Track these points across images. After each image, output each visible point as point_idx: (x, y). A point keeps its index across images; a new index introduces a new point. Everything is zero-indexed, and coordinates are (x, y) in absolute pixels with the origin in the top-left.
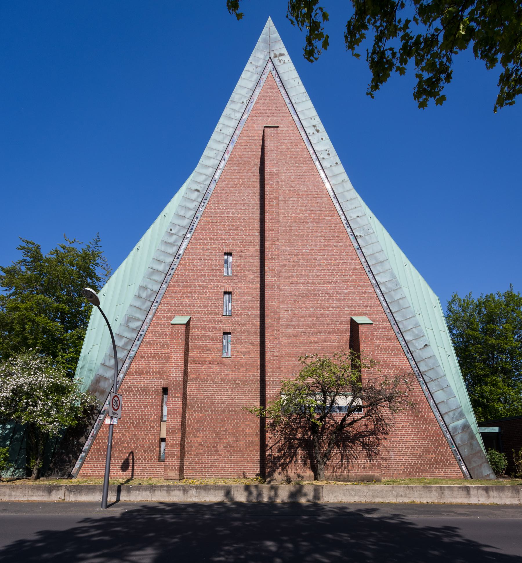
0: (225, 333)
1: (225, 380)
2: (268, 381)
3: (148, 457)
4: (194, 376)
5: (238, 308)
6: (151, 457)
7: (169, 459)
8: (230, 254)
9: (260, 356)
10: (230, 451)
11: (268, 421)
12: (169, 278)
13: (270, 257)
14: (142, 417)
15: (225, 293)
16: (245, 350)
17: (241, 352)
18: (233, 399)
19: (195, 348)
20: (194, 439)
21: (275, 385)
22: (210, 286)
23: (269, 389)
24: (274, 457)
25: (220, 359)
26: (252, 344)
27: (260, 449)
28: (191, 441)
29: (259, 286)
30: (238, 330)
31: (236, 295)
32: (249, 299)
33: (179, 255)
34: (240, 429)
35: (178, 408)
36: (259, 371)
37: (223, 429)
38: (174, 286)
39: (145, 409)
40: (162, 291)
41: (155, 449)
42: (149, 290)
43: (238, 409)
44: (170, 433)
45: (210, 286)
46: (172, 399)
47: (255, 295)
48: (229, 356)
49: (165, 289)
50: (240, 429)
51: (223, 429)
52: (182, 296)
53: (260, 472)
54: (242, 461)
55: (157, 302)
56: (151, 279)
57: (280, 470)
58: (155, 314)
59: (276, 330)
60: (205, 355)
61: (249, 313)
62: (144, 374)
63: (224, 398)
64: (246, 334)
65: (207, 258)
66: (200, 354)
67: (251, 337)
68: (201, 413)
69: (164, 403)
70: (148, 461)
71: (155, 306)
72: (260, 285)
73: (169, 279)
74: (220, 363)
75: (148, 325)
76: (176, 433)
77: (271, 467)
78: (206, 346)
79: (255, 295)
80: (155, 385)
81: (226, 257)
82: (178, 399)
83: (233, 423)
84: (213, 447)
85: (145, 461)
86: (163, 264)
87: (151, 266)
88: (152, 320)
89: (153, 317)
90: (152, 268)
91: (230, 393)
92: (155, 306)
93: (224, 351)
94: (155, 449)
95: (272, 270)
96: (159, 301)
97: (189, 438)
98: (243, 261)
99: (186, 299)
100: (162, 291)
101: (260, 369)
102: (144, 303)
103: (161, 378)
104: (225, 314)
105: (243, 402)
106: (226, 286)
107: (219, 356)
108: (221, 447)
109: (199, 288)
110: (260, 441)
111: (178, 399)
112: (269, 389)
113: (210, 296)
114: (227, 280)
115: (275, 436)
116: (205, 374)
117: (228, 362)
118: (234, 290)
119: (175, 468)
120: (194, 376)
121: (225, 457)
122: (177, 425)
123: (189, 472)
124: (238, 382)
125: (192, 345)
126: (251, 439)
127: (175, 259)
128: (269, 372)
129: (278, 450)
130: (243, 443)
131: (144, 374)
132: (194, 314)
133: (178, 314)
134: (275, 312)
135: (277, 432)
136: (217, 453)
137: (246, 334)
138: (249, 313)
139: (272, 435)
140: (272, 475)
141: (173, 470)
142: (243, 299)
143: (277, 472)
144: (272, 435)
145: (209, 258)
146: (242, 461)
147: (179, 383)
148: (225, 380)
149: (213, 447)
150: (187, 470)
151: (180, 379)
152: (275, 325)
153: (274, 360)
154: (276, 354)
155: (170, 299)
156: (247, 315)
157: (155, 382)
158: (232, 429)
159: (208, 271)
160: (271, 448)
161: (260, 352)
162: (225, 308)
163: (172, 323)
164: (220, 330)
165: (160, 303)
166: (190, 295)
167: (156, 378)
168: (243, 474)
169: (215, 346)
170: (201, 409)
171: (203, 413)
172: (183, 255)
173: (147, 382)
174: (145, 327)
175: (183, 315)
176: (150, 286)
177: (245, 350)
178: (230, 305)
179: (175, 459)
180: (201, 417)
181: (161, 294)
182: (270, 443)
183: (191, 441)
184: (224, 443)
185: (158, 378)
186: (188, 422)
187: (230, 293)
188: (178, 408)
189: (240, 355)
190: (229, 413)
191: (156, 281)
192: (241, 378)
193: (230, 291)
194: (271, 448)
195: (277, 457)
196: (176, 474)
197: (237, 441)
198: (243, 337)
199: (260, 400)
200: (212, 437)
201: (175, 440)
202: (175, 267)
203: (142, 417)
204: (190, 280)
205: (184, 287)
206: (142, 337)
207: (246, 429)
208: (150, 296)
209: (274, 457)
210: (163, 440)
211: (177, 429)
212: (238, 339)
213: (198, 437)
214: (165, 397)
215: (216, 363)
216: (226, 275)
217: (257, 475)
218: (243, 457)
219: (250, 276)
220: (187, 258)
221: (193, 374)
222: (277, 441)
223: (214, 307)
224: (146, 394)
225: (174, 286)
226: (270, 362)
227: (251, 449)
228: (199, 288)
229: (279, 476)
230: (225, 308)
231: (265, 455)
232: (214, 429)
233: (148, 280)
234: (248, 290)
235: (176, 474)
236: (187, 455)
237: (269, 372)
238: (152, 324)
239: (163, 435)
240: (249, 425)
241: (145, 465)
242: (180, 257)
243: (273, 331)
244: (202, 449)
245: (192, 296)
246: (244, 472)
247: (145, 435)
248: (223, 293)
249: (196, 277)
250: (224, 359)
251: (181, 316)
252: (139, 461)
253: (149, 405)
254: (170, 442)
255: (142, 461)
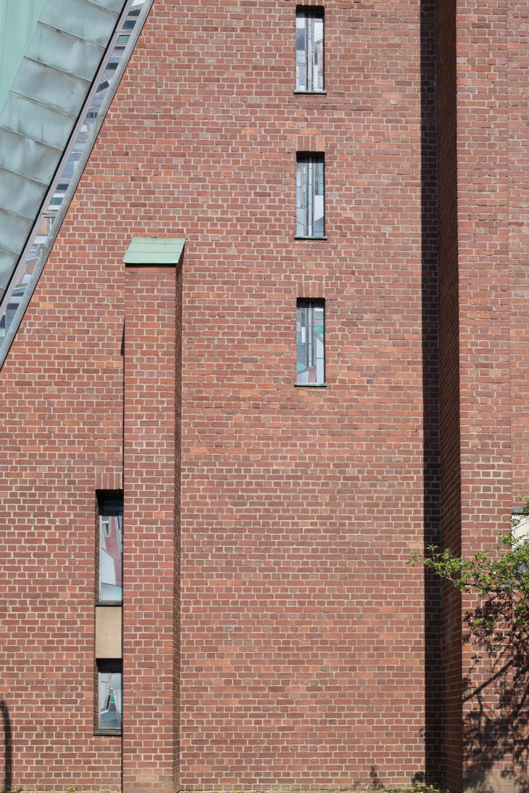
0: (304, 302)
1: (308, 465)
2: (470, 467)
3: (59, 722)
4: (203, 450)
5: (350, 214)
6: (68, 722)
7: (138, 730)
8: (316, 12)
9: (425, 383)
10: (328, 702)
11: (472, 601)
12: (101, 100)
13: (474, 18)
14: (32, 589)
15: (303, 157)
16: (373, 363)
17: (360, 369)
18: (337, 531)
19: (201, 354)
20: (209, 662)
21: (492, 482)
22: (248, 131)
23: (472, 496)
24: (488, 721)
25: (290, 391)
26: (398, 340)
27: (427, 695)
28: (199, 669)
29: (419, 134)
30: (350, 290)
31: (340, 166)
32: (385, 179)
33: (136, 13)
34: (361, 629)
35: (160, 558)
36: (421, 433)
37: (304, 630)
38: (121, 129)
39: (41, 562)
40: (80, 147)
41: (79, 695)
42: (31, 143)
43: (353, 565)
44: (138, 643)
45: (248, 131)
46: (138, 529)
47: (406, 165)
48: (320, 381)
49: (91, 139)
50: (361, 629)
51: (304, 630)
52: (149, 165)
53: (427, 767)
54: (370, 735)
55: (63, 187)
56: (35, 102)
57: (507, 761)
58: (58, 230)
59: (494, 288)
60: (238, 380)
61: (387, 230)
62: (32, 443)
63: (305, 525)
64: (378, 304)
65: (234, 23)
66: (220, 373)
67: (395, 317)
68: (229, 577)
69: (103, 544)
70: (59, 735)
71: (58, 201)
72: (423, 128)
73: (105, 101)
74: (289, 407)
75: (36, 269)
76: (158, 644)
77: (477, 752)
78: (241, 345)
79: (406, 165)
80: (71, 482)
81: (301, 22)
82: (159, 529)
83: (337, 610)
84: (272, 689)
85: (49, 736)
86: (77, 45)
87: (33, 52)
88: (48, 251)
89: (52, 242)
90: (38, 62)
91: (324, 510)
92: (58, 201)
93: (300, 366)
94: (79, 695)
95: (481, 69)
96: (72, 183)
97: (195, 658)
98: (363, 40)
99: (166, 178)
100: (80, 147)
101: (425, 428)
102: (15, 192)
103: (91, 457)
104: (300, 234)
105: (370, 539)
106: (306, 131)
107: (287, 380)
108: (298, 690)
109: (208, 136)
110: (427, 669)
111: (159, 529)
112: (472, 496)
113: (251, 169)
114: (309, 108)
115: (492, 654)
116: (238, 445)
117: (316, 401)
118: (333, 146)
119: (158, 758)
120: (203, 450)
121: (314, 722)
122: (157, 615)
123: (195, 768)
124: (351, 471)
125: (190, 341)
126: (396, 662)
127: (120, 29)
128: (471, 437)
129: (502, 699)
130: (370, 674)
131: (32, 443)
132: (194, 232)
133: (140, 232)
134: (491, 224)
135: (500, 638)
136: (285, 709)
137: (378, 304)
138: (387, 230)
139: (483, 650)
140: (482, 778)
141: (154, 765)
142: (365, 180)
143: (496, 770)
144: (483, 650)
145: (242, 23)
146: (370, 735)
147: (161, 473)
148: (308, 465)
149: (272, 689)
150: (191, 762)
151: (163, 459)
152: (493, 271)
153: (490, 395)
154: (495, 373)
155: (109, 175)
156: (379, 236)
157: (71, 469)
158: (333, 629)
159: (240, 75)
160: (478, 691)
161: (425, 369)
162: (301, 213)
163: (128, 259)
164: (288, 291)
165: (76, 190)
166: (179, 162)
167: (72, 456)
168: (373, 774)
169: (270, 348)
170: (228, 563)
171: (238, 577)
172: (150, 13)
173: (43, 469)
174: (26, 278)
175: (157, 234)
176: (33, 129)
177: (373, 363)
178: (319, 200)
179: (159, 730)
180: (229, 590)
181: (75, 157)
182: (478, 677)
183: (199, 669)
184: (309, 675)
185: (81, 456)
186: (189, 609)
187: (317, 157)
188: (160, 558)
189: (356, 377)
190: (324, 577)
191: (54, 110)
192: (360, 459)
193: (319, 148)
194: (478, 691)
195: (497, 722)
196: (162, 778)
197: (353, 669)
198: (367, 317)
199: (426, 532)
200: (268, 656)
201: (153, 666)
202: (122, 57)
203: (32, 589)
204: (178, 105)
205: (159, 131)
206: (17, 314)
207: (380, 629)
208: (37, 164)
209: (488, 721)
210: (108, 665)
211: (158, 629)
212: (351, 323)
213: (221, 656)
214: (103, 521)
215: (276, 405)
216: (302, 89)
217: (418, 777)
218: (370, 722)
219: (386, 95)
220: (162, 21)
221: (199, 444)
222: (499, 668)
223: (263, 205)
224: (41, 513)
225: (121, 129)
226: (475, 402)
227: (398, 694)
228: (208, 136)
229: (502, 781)
230: (301, 213)
231: (461, 714)
232: (276, 629)
233: (26, 104)
234: (383, 146)
235: (162, 778)
236: (187, 716)
237: (471, 437)
238: (51, 266)
239: (111, 650)
240: (389, 616)
241: (50, 749)
242: (139, 20)
243: (484, 293)
244: (237, 696)
245: (187, 167)
246: (373, 768)
247: (45, 649)
248: (293, 158)
249: (198, 97)
250: (303, 392)
251: (149, 240)
252: (29, 736)
253: (52, 549)
254: (138, 672)
255: (39, 735)
